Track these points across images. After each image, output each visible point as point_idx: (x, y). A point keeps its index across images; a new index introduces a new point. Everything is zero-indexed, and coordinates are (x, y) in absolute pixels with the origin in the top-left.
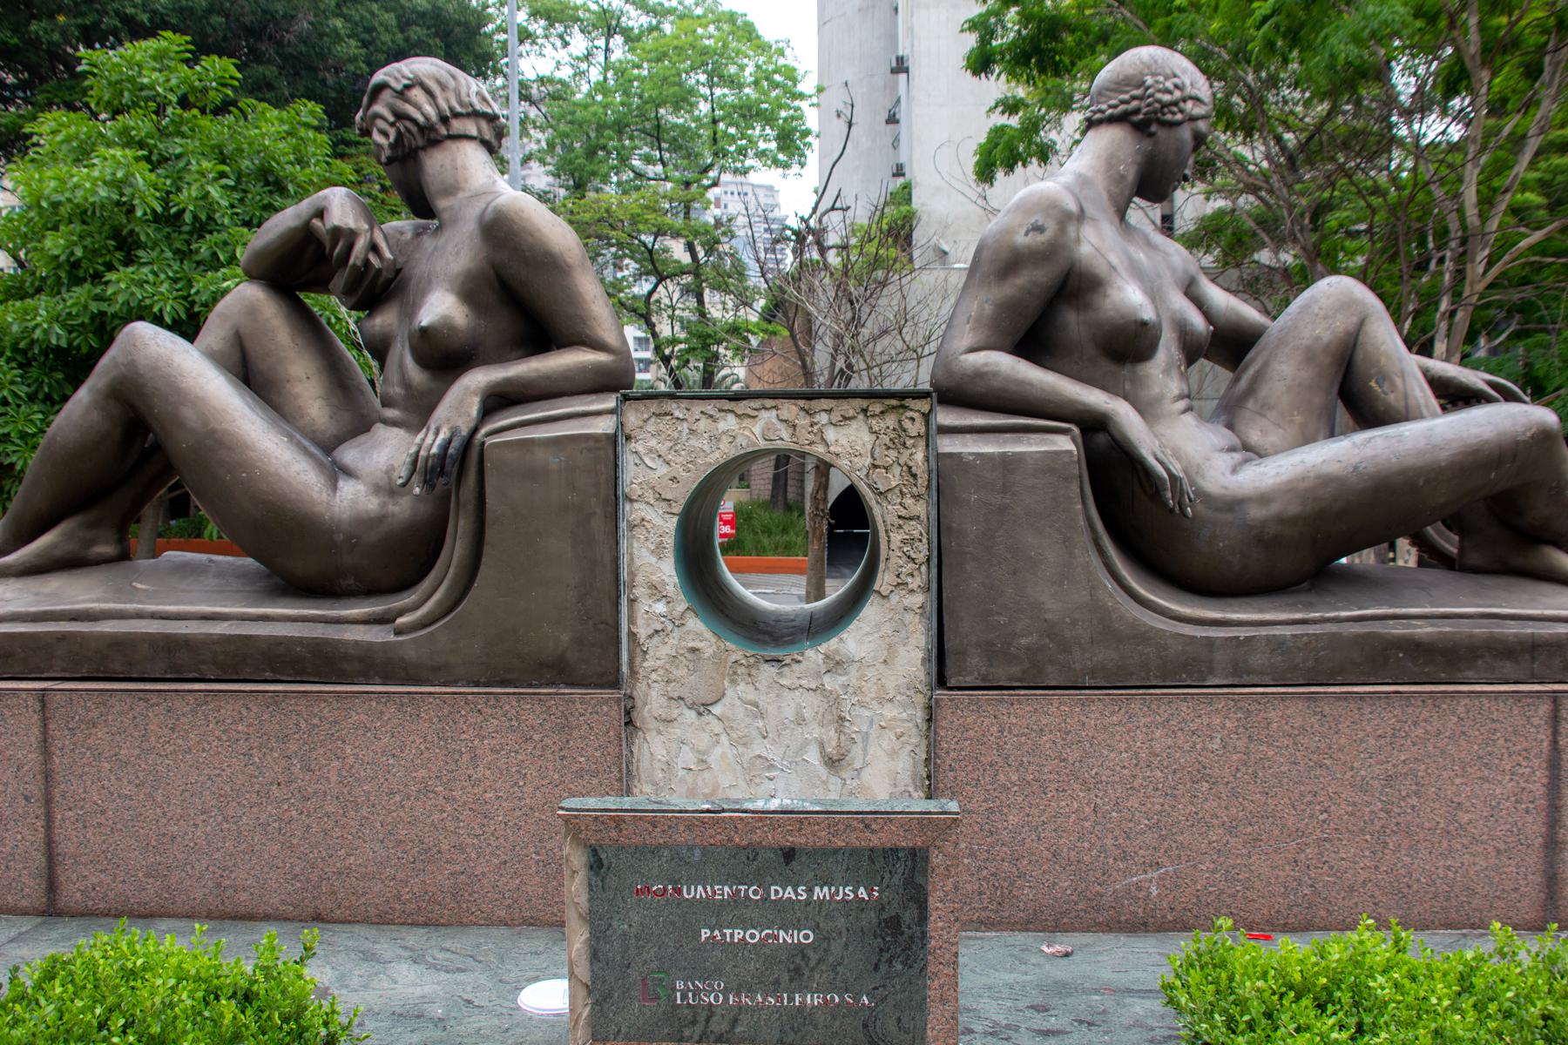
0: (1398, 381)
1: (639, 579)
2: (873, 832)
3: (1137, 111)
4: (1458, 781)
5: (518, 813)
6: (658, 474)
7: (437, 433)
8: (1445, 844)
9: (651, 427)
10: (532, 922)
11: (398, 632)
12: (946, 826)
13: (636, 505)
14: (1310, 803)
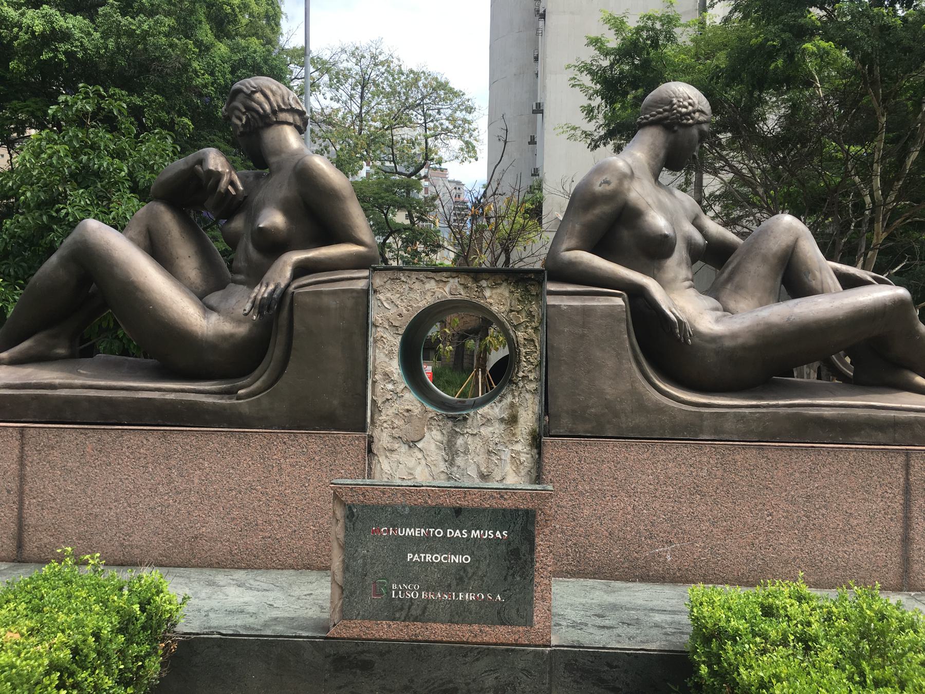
0: (817, 274)
1: (379, 370)
2: (505, 499)
3: (667, 118)
4: (850, 500)
5: (304, 502)
6: (391, 312)
7: (267, 286)
8: (843, 537)
9: (388, 286)
10: (309, 567)
11: (239, 398)
12: (544, 498)
13: (379, 329)
14: (760, 510)
